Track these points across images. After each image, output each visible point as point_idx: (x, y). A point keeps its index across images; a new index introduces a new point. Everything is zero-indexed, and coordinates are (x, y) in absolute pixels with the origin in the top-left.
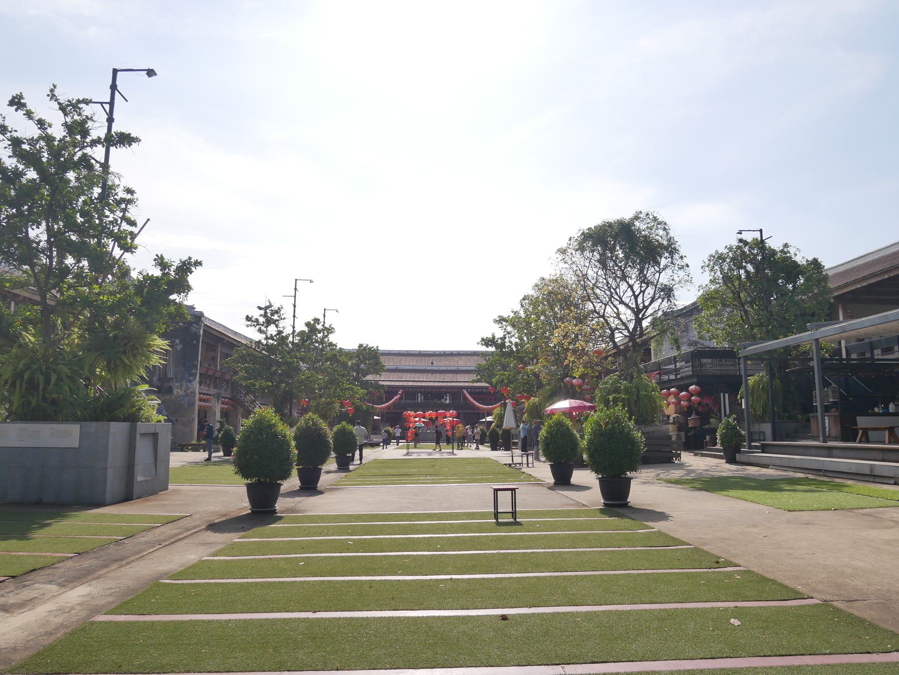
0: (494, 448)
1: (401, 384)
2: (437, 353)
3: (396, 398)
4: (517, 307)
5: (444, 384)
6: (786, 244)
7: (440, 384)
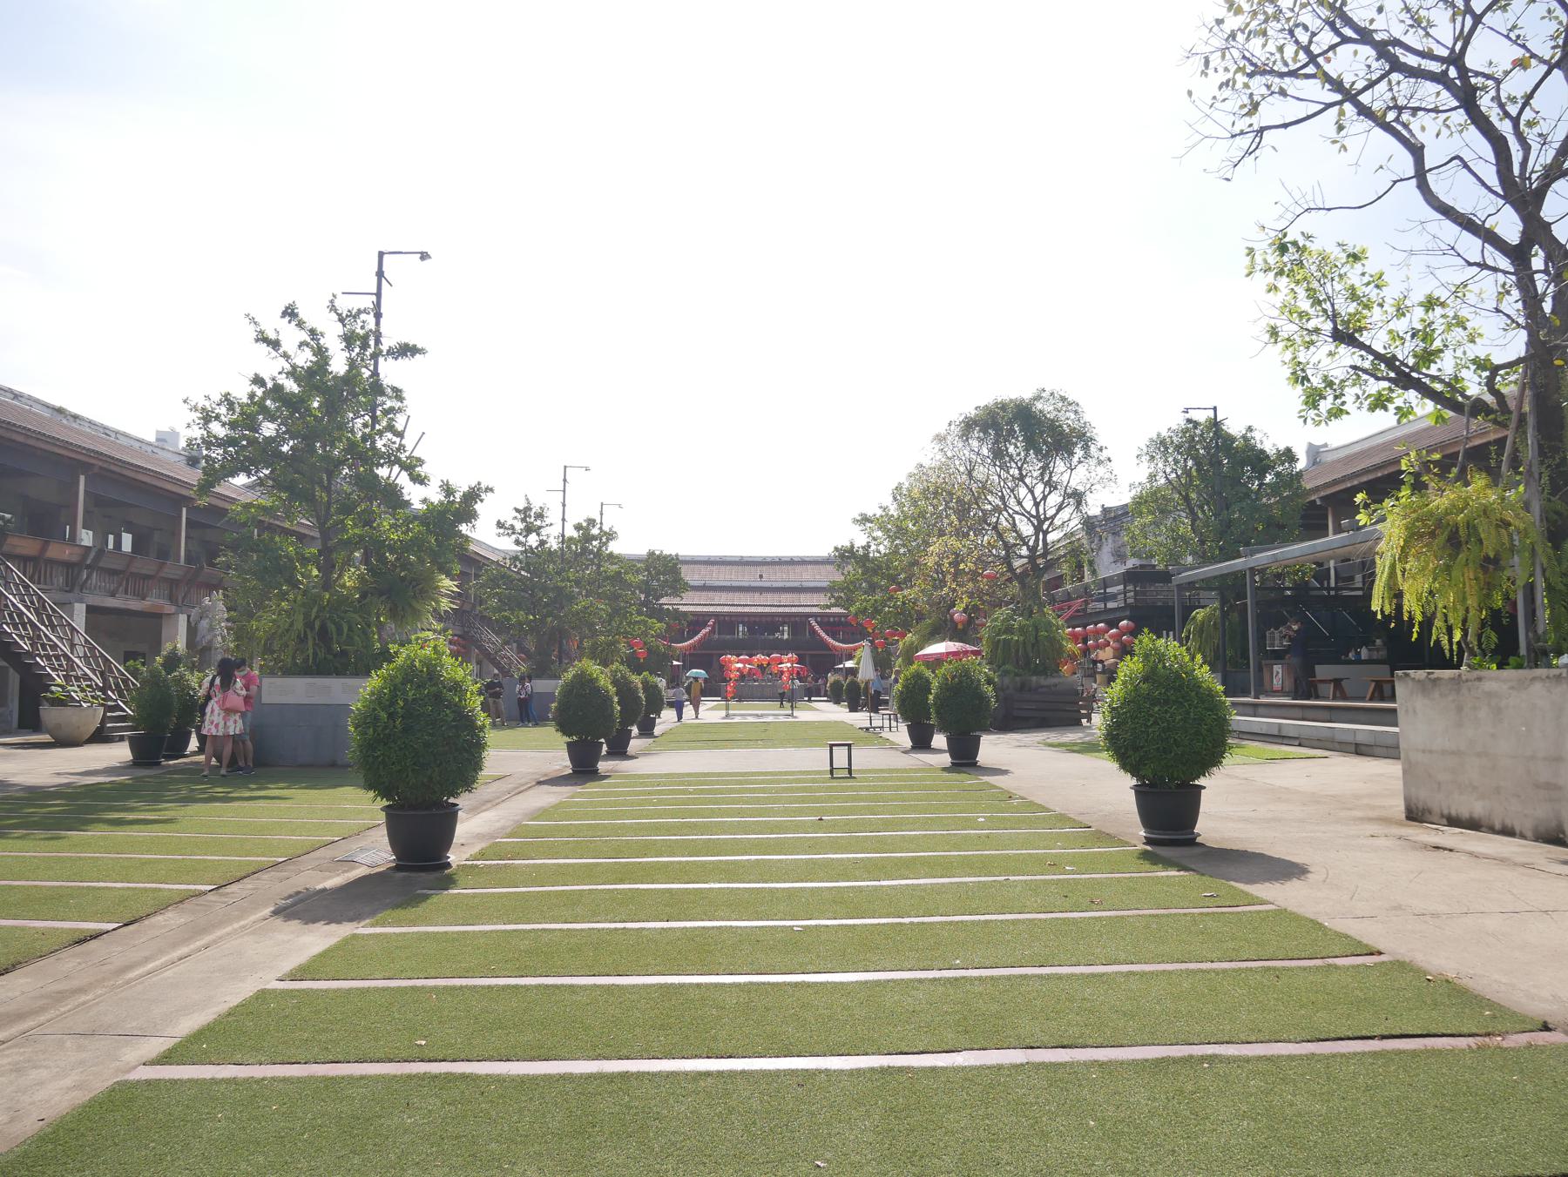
0: (853, 709)
1: (711, 609)
2: (769, 560)
3: (704, 631)
4: (888, 500)
5: (780, 610)
6: (1250, 427)
7: (774, 610)
